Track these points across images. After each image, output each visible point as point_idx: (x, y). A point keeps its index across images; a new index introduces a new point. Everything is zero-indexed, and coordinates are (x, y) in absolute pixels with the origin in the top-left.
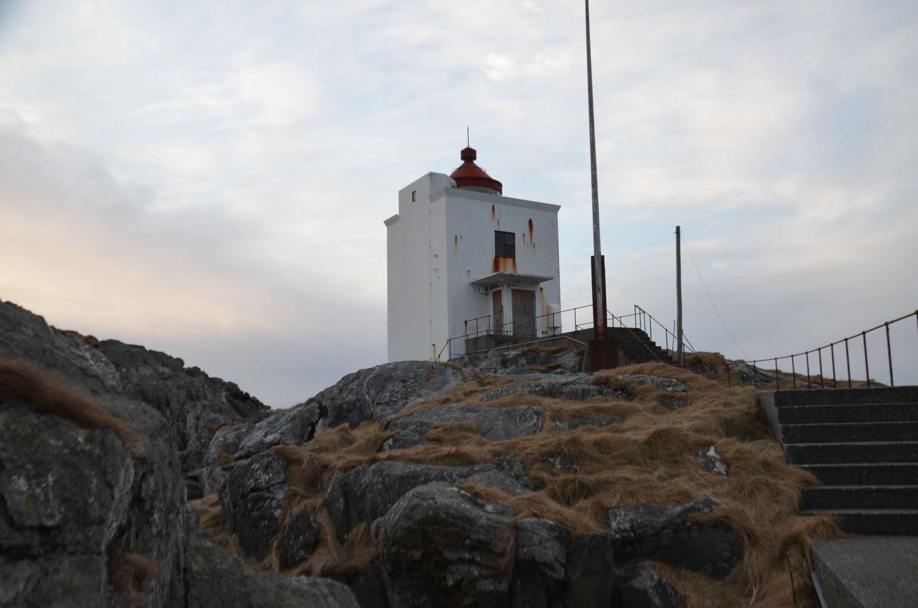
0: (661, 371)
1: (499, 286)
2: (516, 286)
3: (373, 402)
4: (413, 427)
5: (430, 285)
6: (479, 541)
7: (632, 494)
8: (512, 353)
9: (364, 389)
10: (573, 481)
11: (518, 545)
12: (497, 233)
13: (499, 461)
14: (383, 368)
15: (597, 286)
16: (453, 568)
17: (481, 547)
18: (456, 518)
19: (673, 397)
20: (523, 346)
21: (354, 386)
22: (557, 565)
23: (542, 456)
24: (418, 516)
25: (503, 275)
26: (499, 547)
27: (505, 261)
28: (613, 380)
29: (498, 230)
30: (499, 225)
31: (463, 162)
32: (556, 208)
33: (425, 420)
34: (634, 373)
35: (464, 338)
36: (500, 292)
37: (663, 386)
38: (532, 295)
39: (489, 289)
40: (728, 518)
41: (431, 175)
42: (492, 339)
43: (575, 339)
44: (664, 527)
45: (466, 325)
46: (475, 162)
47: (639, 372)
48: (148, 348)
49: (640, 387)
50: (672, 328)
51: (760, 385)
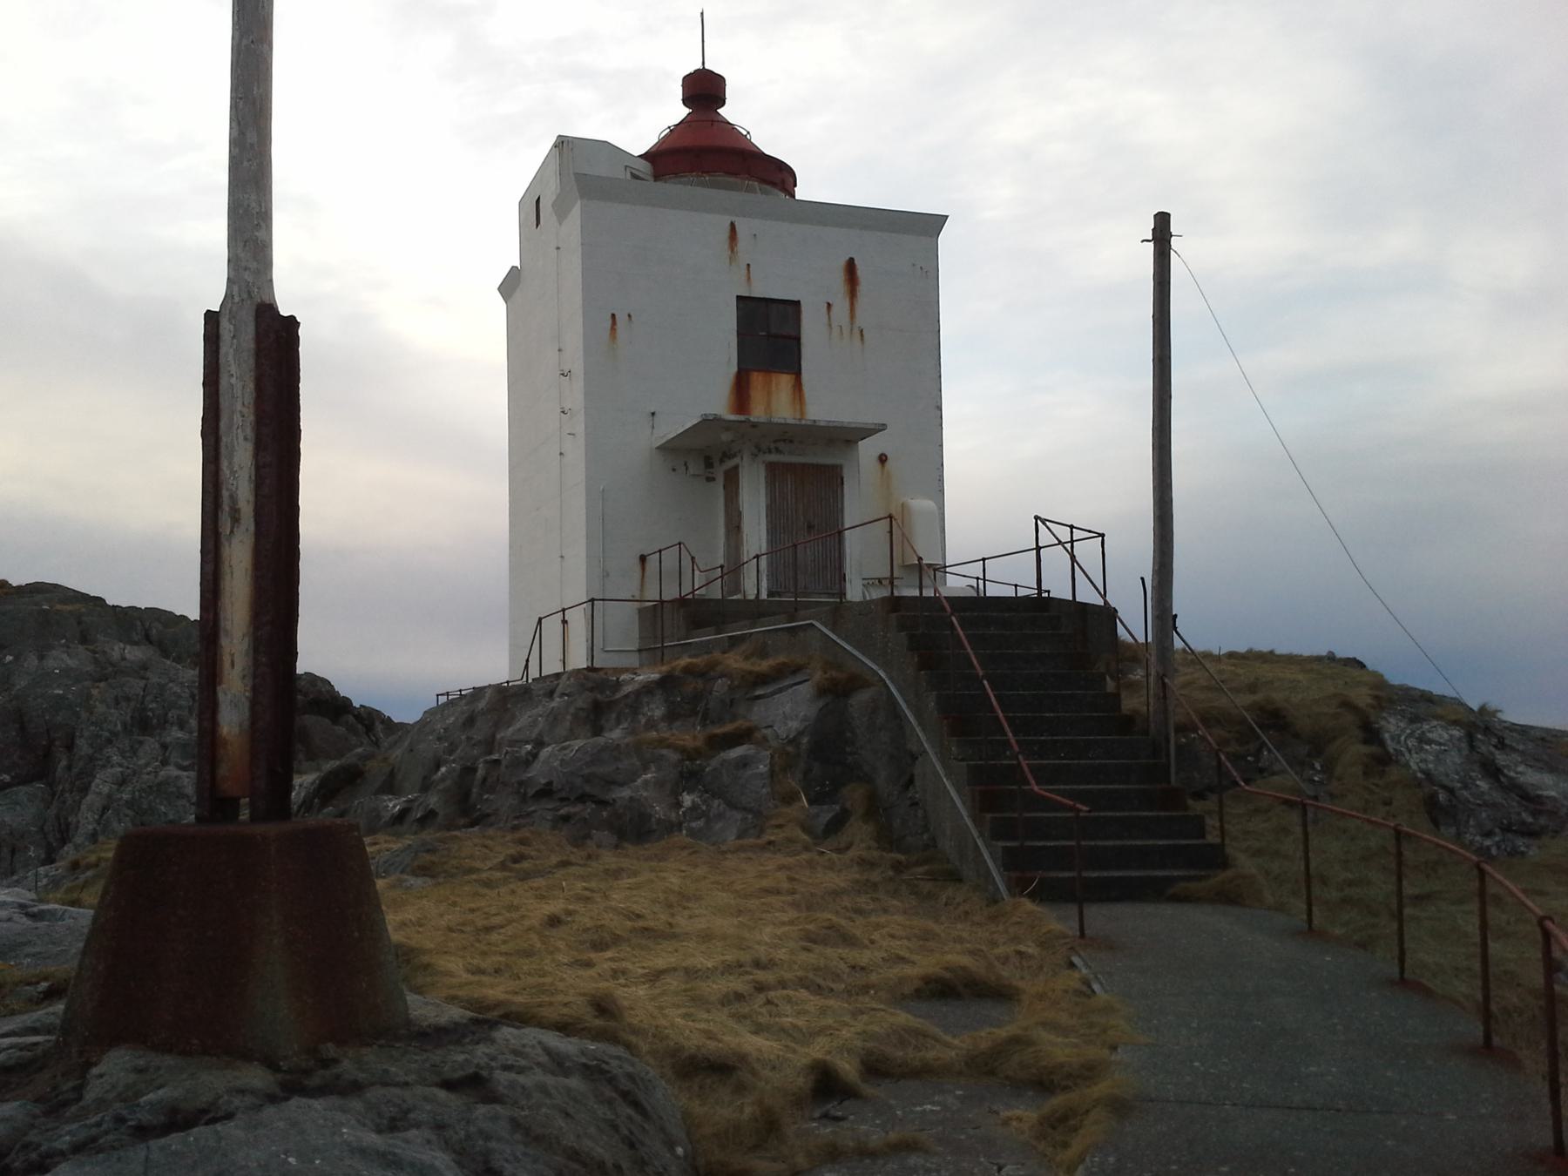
1: (734, 456)
2: (778, 451)
5: (561, 454)
12: (747, 305)
15: (225, 494)
29: (746, 294)
30: (749, 278)
31: (685, 111)
32: (933, 224)
35: (637, 605)
36: (736, 468)
38: (832, 479)
39: (716, 464)
43: (833, 631)
45: (643, 569)
46: (723, 111)
48: (110, 602)
51: (1494, 851)
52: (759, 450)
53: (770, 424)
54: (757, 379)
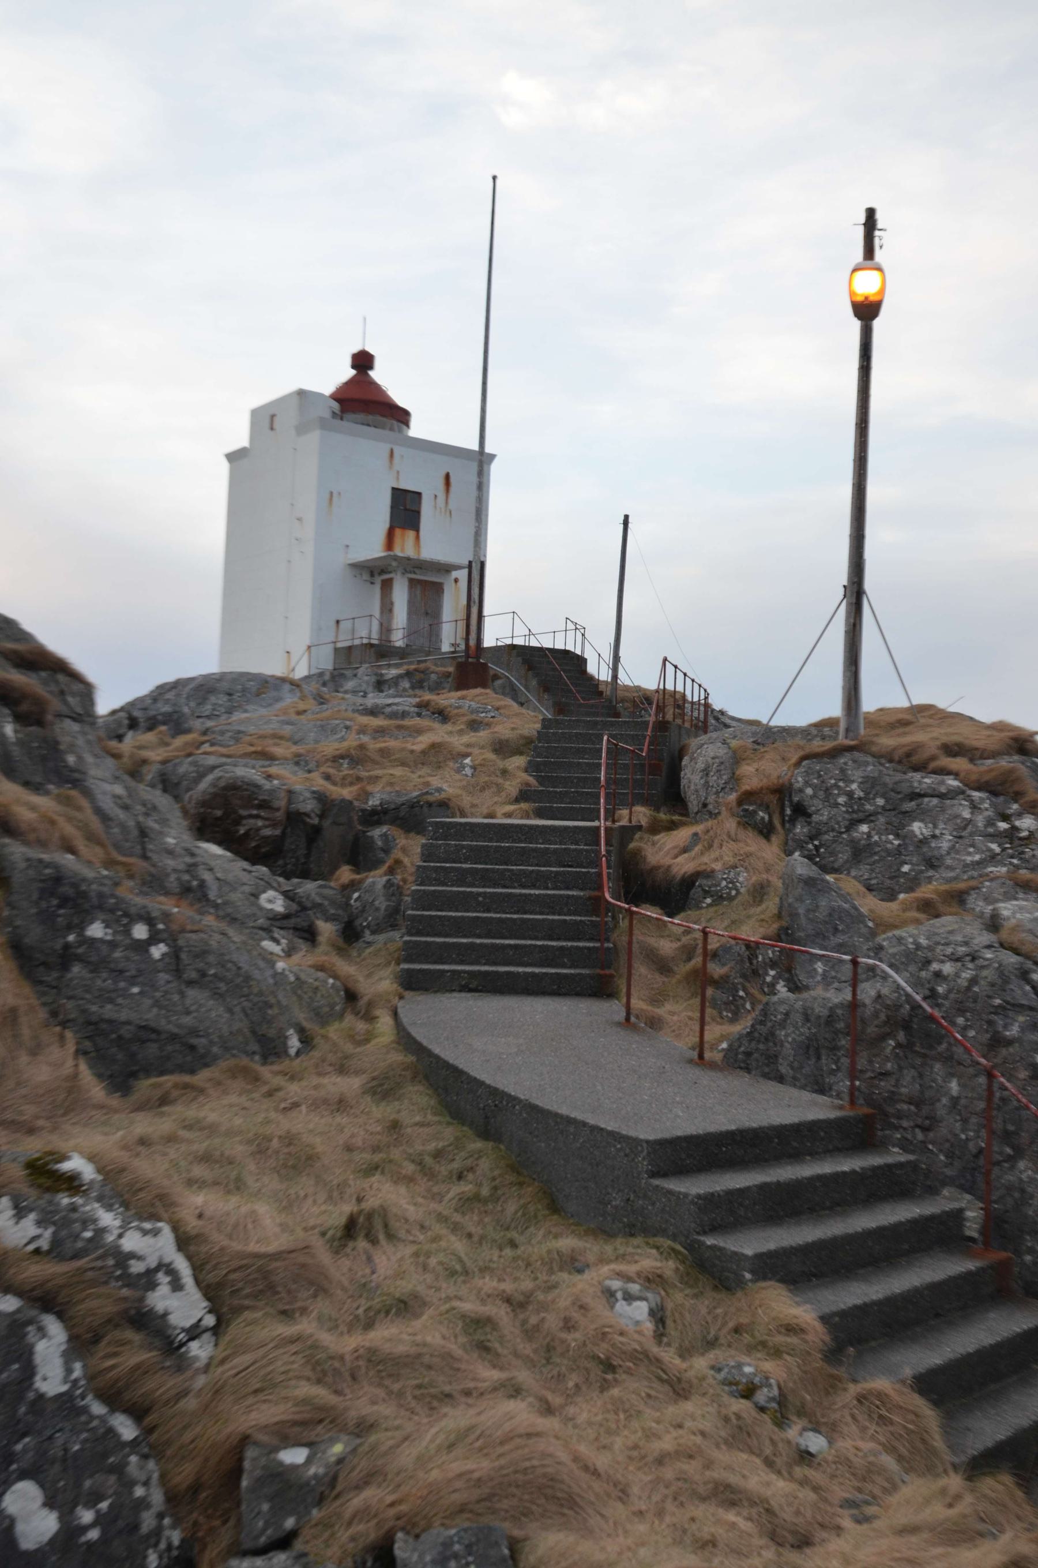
0: (481, 698)
1: (390, 572)
2: (415, 573)
3: (193, 714)
4: (230, 734)
6: (264, 800)
7: (391, 784)
8: (394, 672)
9: (183, 701)
10: (351, 775)
11: (290, 802)
13: (298, 760)
14: (207, 677)
16: (244, 822)
17: (264, 805)
18: (248, 785)
19: (481, 722)
20: (411, 663)
21: (170, 696)
22: (313, 815)
23: (334, 757)
24: (222, 783)
25: (396, 558)
26: (276, 804)
27: (403, 536)
28: (433, 704)
33: (242, 728)
34: (459, 698)
36: (391, 580)
37: (477, 711)
40: (449, 799)
41: (301, 394)
42: (373, 650)
44: (403, 804)
46: (371, 373)
47: (463, 698)
49: (456, 711)
50: (607, 655)
52: (405, 571)
53: (418, 560)
54: (398, 532)
